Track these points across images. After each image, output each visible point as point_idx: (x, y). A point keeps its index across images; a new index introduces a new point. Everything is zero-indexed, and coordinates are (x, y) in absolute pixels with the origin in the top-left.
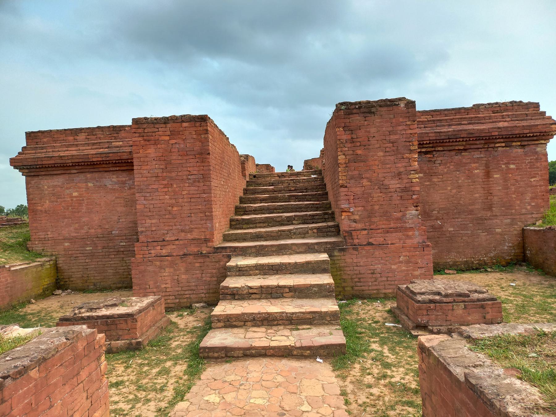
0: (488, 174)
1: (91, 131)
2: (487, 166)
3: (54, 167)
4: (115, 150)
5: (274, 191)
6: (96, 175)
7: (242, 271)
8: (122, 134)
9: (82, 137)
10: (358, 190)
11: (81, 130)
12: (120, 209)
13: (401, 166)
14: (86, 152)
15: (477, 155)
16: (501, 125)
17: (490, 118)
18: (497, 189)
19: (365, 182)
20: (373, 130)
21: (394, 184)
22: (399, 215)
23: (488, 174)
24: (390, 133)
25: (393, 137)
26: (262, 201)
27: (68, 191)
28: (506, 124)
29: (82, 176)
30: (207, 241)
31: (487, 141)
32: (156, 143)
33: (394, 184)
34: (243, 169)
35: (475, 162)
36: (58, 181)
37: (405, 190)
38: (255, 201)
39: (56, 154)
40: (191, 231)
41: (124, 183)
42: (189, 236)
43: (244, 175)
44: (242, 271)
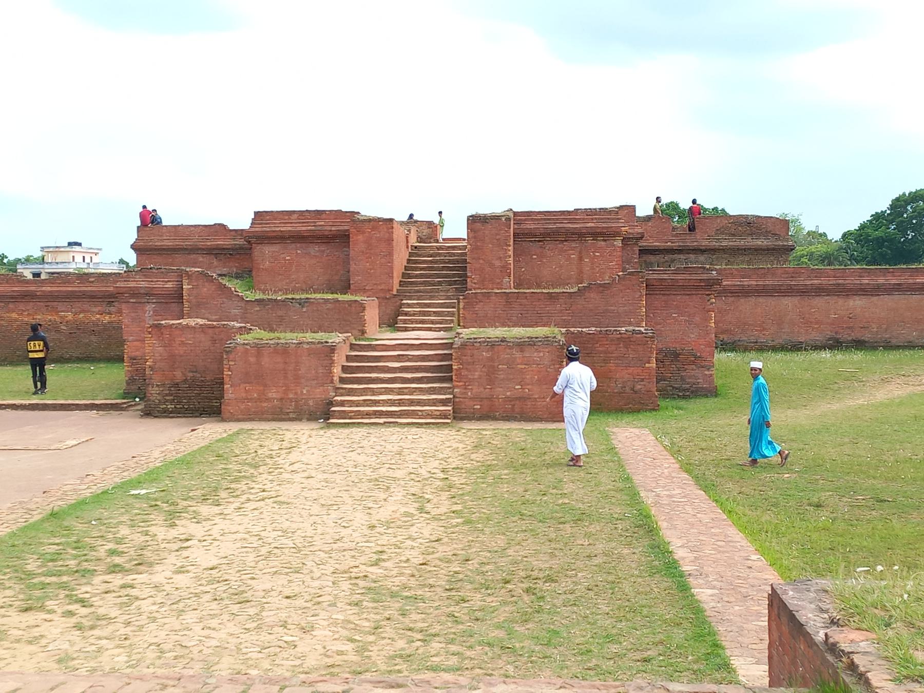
0: (581, 259)
1: (301, 213)
2: (580, 253)
3: (275, 238)
4: (319, 228)
5: (431, 262)
6: (304, 245)
7: (409, 305)
8: (324, 216)
9: (295, 216)
10: (478, 266)
11: (294, 212)
12: (319, 270)
13: (501, 254)
14: (299, 229)
15: (574, 245)
16: (589, 225)
17: (584, 219)
18: (586, 269)
19: (481, 261)
20: (487, 232)
21: (497, 263)
22: (498, 281)
23: (581, 259)
24: (497, 234)
25: (498, 237)
26: (422, 269)
27: (283, 256)
28: (593, 225)
29: (293, 245)
30: (389, 290)
31: (580, 235)
32: (364, 233)
33: (497, 263)
34: (407, 242)
35: (572, 250)
36: (275, 248)
37: (503, 267)
38: (416, 269)
39: (278, 229)
40: (380, 284)
41: (323, 251)
42: (380, 287)
43: (408, 247)
44: (409, 305)
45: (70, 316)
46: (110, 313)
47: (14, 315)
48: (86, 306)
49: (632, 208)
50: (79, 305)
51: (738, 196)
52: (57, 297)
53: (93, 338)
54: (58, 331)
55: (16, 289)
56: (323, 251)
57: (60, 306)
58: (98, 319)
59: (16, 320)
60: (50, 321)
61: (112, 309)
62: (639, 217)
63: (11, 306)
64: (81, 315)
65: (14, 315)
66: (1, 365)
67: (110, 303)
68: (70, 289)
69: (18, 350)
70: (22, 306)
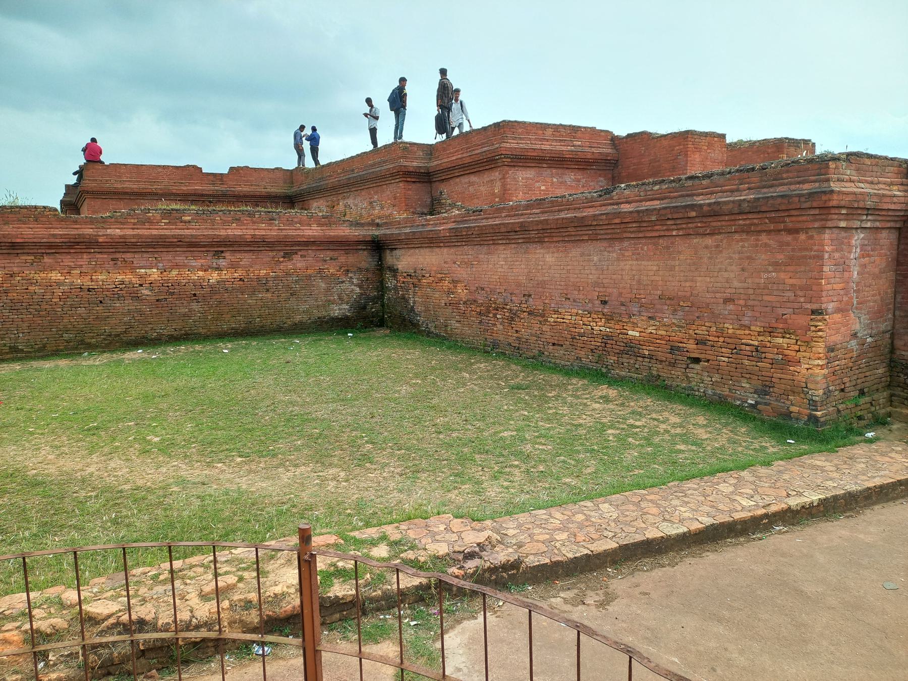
6: (560, 171)
11: (549, 125)
27: (537, 185)
36: (530, 173)
41: (579, 181)
45: (154, 274)
46: (218, 269)
47: (55, 276)
48: (180, 259)
49: (723, 136)
50: (170, 257)
51: (499, 119)
52: (134, 245)
53: (195, 306)
54: (137, 298)
55: (57, 232)
56: (579, 181)
57: (137, 259)
58: (200, 278)
59: (59, 284)
60: (123, 282)
61: (222, 263)
62: (730, 145)
63: (47, 260)
64: (174, 273)
65: (55, 276)
66: (2, 361)
67: (218, 254)
68: (155, 232)
69: (67, 331)
70: (68, 261)
